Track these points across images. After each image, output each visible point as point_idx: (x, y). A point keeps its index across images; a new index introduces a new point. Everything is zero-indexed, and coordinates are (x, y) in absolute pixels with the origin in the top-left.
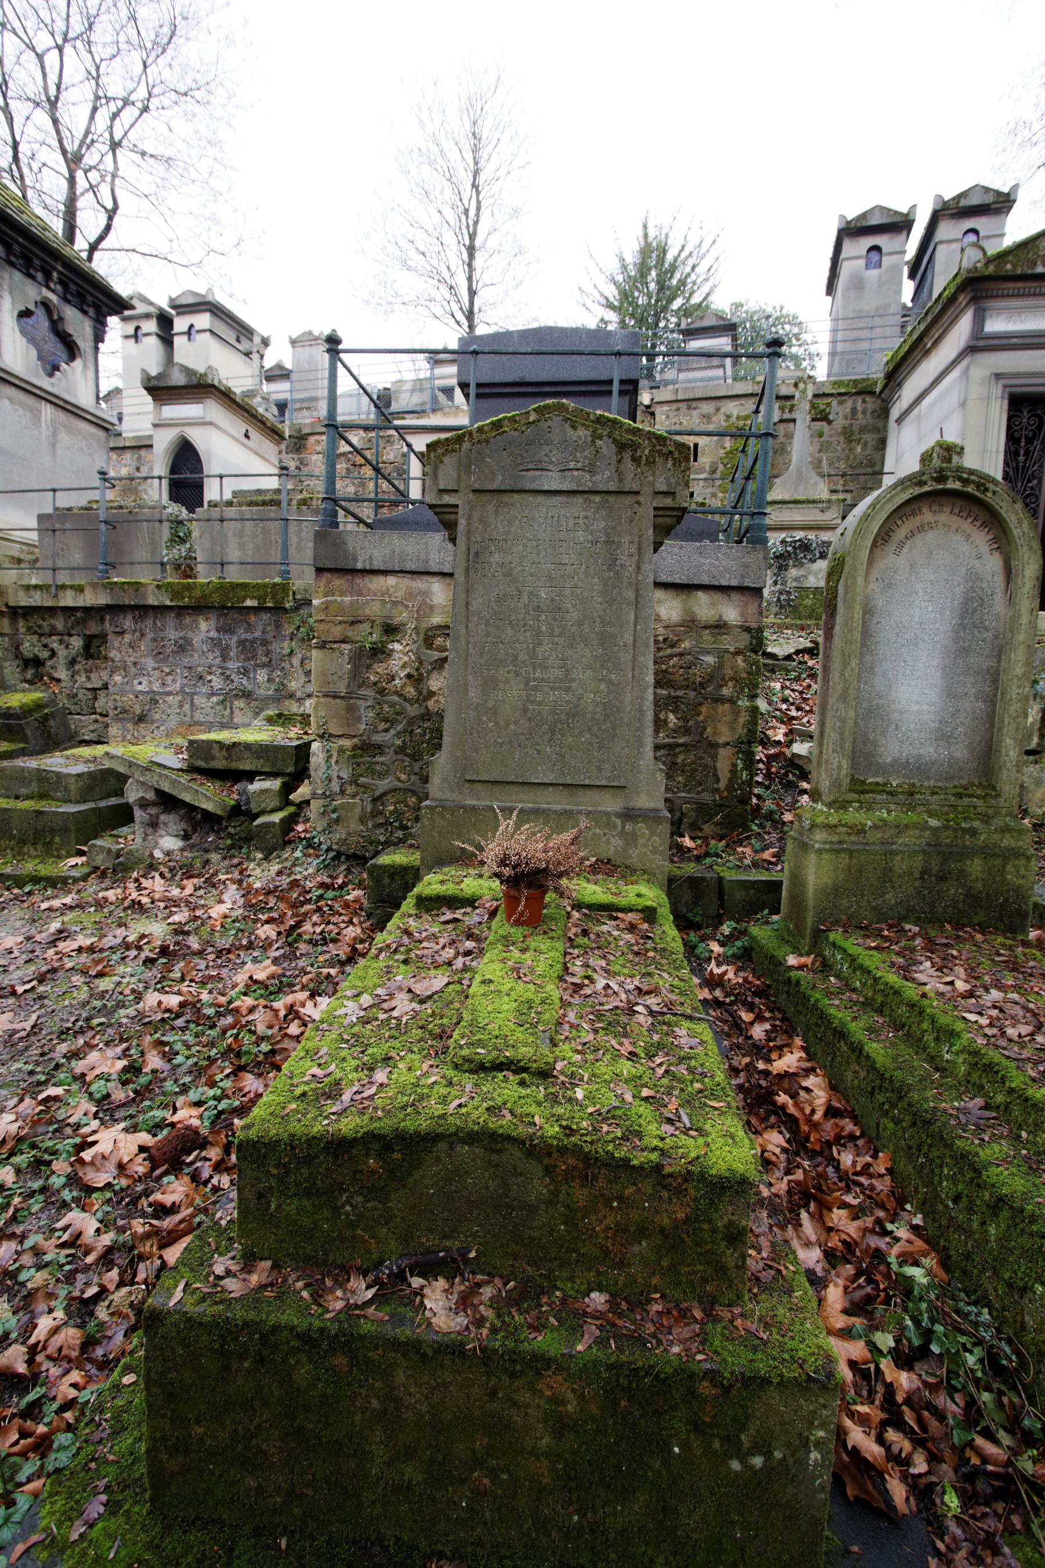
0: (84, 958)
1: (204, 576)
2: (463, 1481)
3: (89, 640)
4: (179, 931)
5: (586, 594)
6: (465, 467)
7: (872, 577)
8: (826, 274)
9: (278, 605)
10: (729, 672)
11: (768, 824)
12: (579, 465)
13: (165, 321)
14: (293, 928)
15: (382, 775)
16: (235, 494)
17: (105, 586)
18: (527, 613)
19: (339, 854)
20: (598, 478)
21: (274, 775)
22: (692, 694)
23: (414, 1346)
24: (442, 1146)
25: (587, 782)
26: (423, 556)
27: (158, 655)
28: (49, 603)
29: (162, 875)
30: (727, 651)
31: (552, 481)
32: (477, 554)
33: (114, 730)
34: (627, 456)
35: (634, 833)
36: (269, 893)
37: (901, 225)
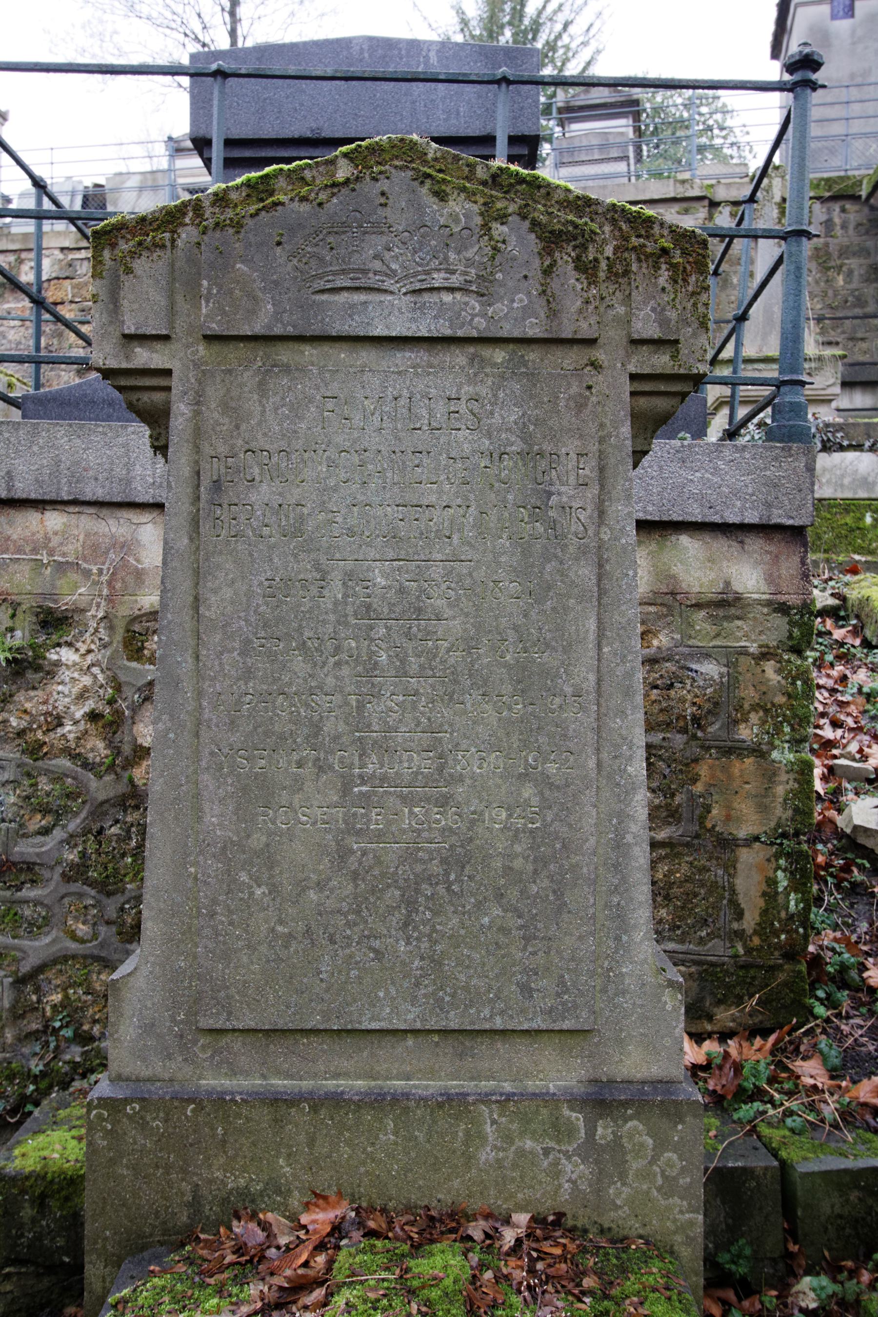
5: (481, 574)
6: (184, 284)
8: (771, 27)
10: (749, 694)
11: (843, 996)
12: (456, 280)
15: (35, 927)
18: (343, 621)
20: (500, 308)
22: (679, 740)
25: (499, 1023)
26: (119, 471)
30: (743, 652)
31: (392, 316)
32: (217, 485)
34: (565, 259)
35: (616, 1144)
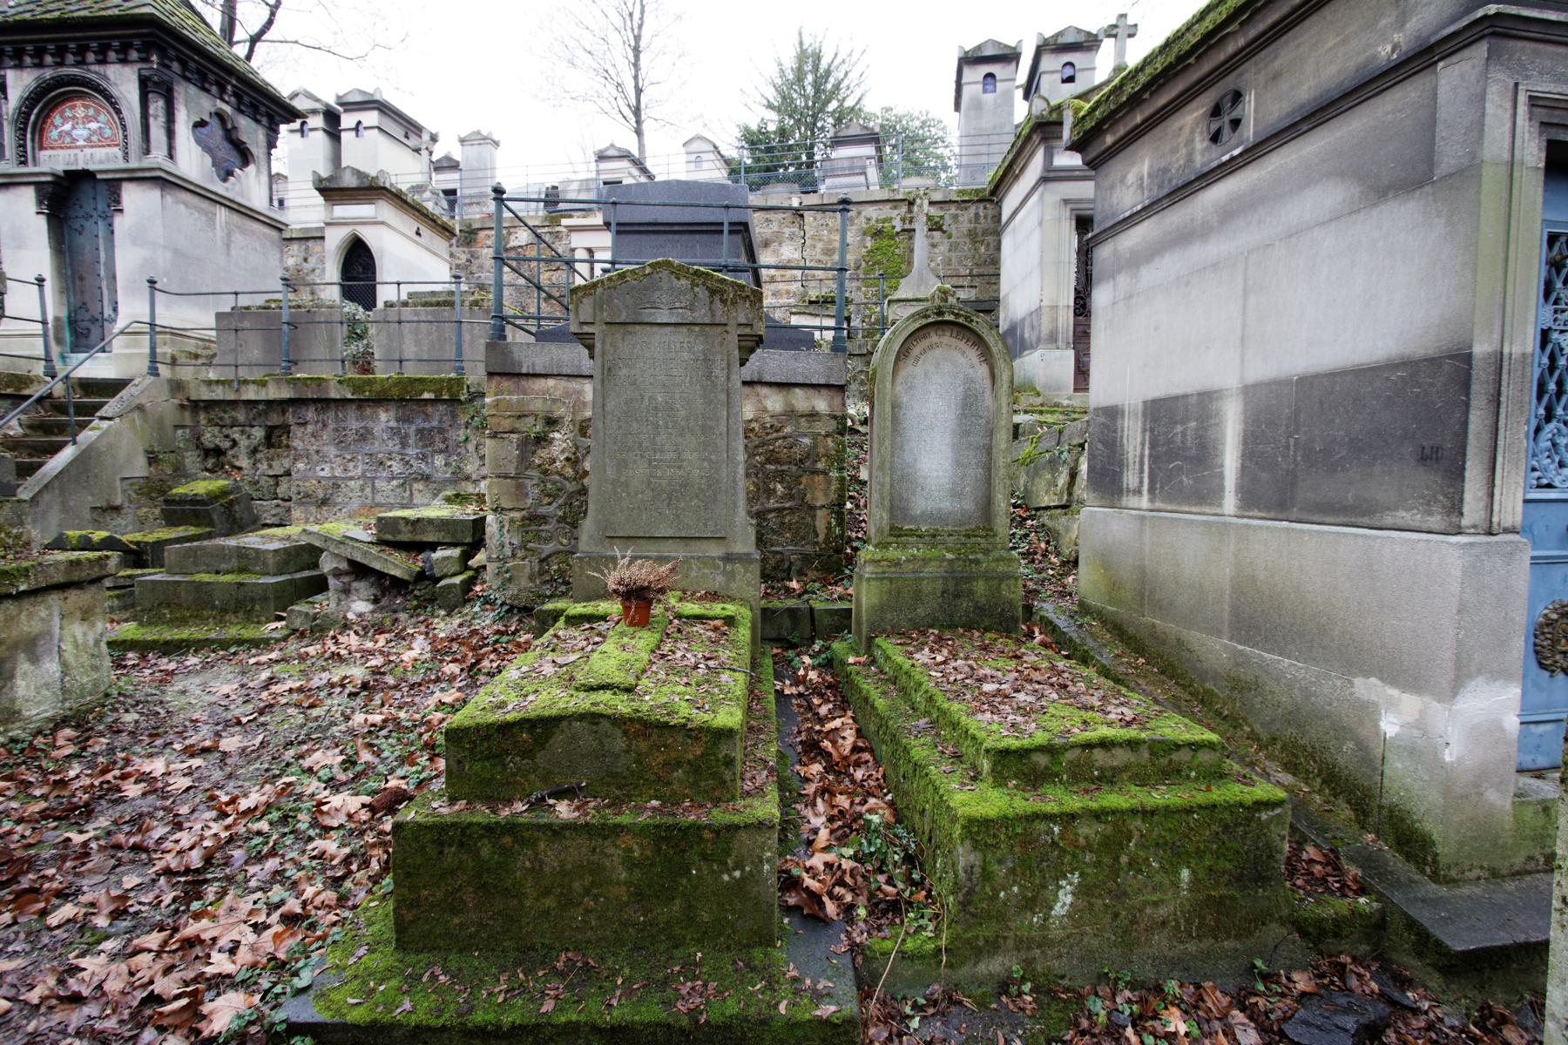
0: (295, 696)
1: (383, 372)
2: (578, 905)
3: (270, 431)
4: (376, 671)
6: (598, 306)
7: (899, 381)
9: (453, 397)
13: (332, 118)
14: (473, 665)
15: (547, 540)
16: (410, 295)
17: (288, 382)
19: (512, 607)
21: (455, 545)
22: (794, 468)
23: (549, 826)
24: (565, 723)
27: (340, 443)
28: (232, 397)
29: (356, 633)
33: (297, 513)
34: (717, 298)
36: (452, 640)
37: (1009, 57)
